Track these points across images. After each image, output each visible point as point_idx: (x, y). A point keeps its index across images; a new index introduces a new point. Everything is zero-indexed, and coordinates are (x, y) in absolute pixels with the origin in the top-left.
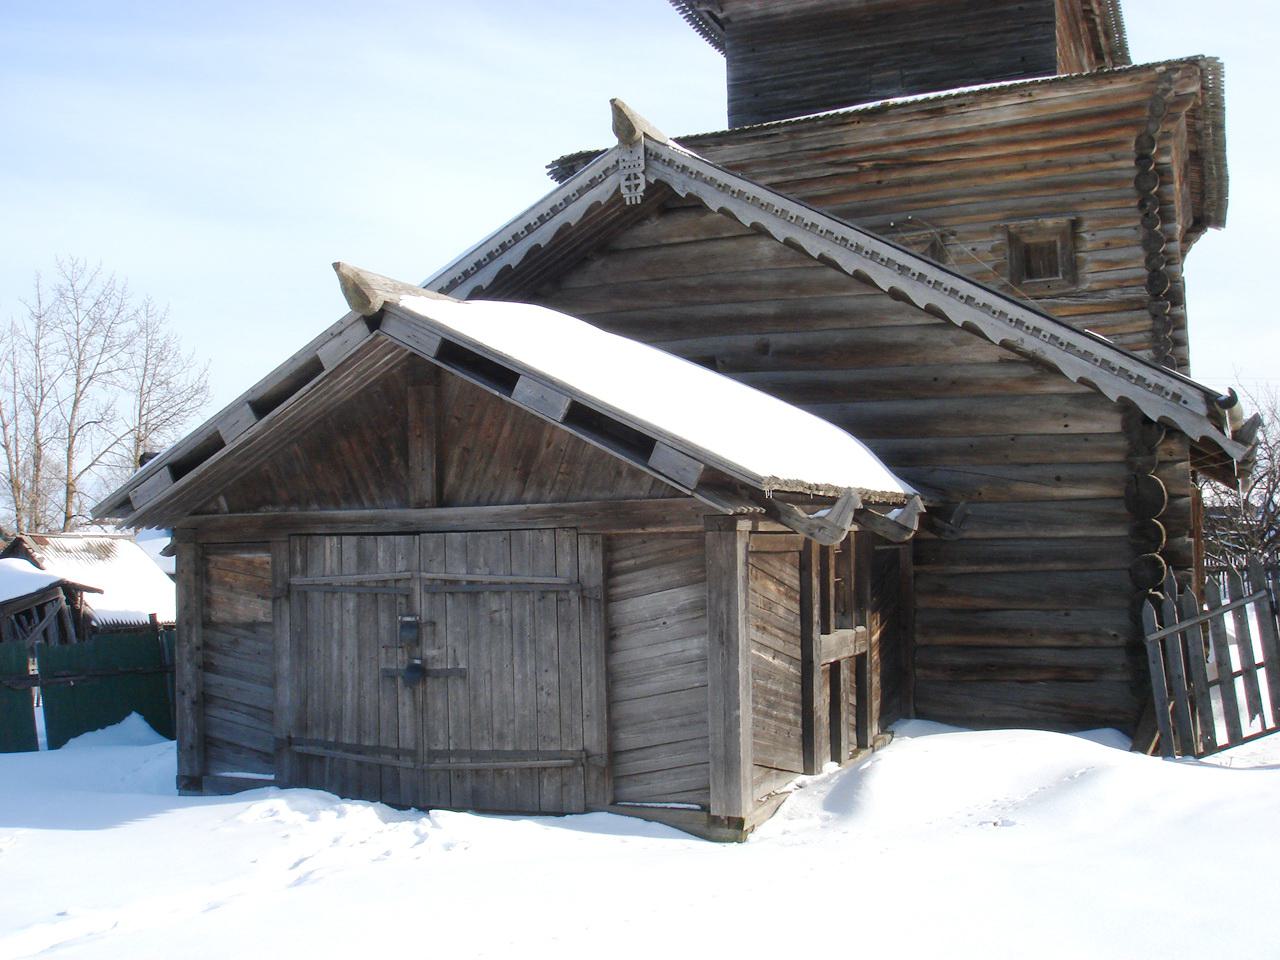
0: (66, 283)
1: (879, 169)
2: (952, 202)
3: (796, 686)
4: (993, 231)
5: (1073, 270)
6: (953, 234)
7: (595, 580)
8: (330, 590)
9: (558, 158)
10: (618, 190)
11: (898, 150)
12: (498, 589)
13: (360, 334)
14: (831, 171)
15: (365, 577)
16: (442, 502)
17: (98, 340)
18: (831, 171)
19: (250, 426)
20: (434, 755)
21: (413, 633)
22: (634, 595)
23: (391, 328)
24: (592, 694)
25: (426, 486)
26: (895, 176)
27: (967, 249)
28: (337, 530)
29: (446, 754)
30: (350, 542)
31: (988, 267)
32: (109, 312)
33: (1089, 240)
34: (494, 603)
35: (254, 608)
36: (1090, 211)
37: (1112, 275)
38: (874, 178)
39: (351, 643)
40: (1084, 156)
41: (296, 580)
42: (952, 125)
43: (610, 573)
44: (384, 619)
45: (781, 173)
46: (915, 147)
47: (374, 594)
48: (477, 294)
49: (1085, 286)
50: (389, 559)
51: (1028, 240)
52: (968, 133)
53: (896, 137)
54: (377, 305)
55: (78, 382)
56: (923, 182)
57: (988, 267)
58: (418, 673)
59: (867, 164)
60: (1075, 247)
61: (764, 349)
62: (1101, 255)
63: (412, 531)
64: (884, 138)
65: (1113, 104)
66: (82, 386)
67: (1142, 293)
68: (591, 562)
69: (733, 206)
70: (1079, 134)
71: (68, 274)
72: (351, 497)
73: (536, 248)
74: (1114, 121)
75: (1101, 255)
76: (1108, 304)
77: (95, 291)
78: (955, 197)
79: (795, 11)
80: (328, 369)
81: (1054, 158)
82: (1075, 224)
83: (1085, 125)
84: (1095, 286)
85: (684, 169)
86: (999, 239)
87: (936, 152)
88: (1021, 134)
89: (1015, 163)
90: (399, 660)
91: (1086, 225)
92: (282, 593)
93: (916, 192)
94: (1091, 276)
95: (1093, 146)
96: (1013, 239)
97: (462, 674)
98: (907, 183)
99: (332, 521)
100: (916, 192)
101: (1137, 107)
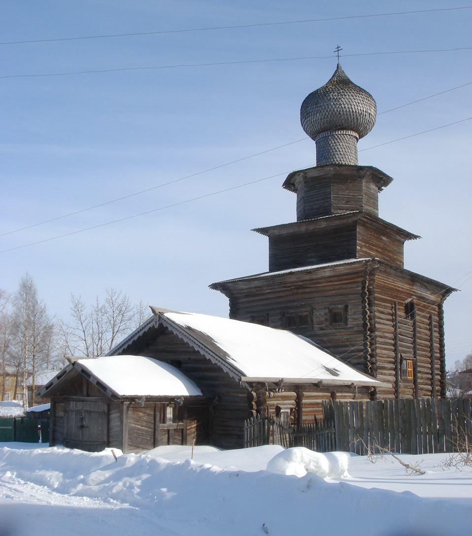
0: (110, 298)
1: (297, 289)
2: (316, 299)
3: (153, 433)
4: (325, 308)
5: (346, 320)
6: (315, 309)
7: (106, 411)
8: (72, 411)
9: (211, 283)
10: (154, 326)
11: (301, 283)
12: (94, 412)
13: (71, 366)
14: (284, 289)
15: (77, 409)
16: (88, 395)
17: (120, 317)
18: (284, 289)
19: (57, 382)
20: (84, 441)
21: (82, 419)
22: (112, 414)
23: (75, 366)
24: (105, 432)
25: (85, 393)
26: (301, 291)
27: (318, 314)
28: (73, 400)
29: (86, 441)
30: (75, 402)
31: (323, 319)
32: (124, 308)
33: (350, 312)
34: (93, 414)
35: (61, 414)
36: (350, 303)
37: (355, 323)
38: (296, 291)
39: (74, 421)
40: (350, 286)
41: (68, 409)
42: (314, 277)
43: (109, 410)
44: (79, 417)
45: (271, 289)
46: (305, 282)
47: (78, 412)
48: (110, 356)
49: (349, 326)
50: (80, 406)
51: (334, 311)
52: (318, 279)
53: (299, 280)
54: (73, 362)
55: (113, 333)
56: (309, 293)
57: (323, 319)
58: (82, 427)
59: (293, 287)
60: (347, 314)
61: (189, 359)
62: (352, 317)
63: (83, 401)
64: (297, 280)
65: (356, 270)
66: (114, 335)
67: (361, 329)
68: (105, 408)
69: (173, 330)
70: (348, 279)
71: (110, 294)
72: (76, 394)
73: (134, 341)
74: (357, 275)
75: (352, 317)
76: (355, 331)
77: (119, 301)
78: (316, 298)
79: (288, 233)
80: (67, 372)
81: (342, 286)
82: (346, 307)
83: (349, 277)
84: (351, 326)
85: (165, 321)
86: (327, 311)
87: (311, 284)
88: (332, 279)
89: (332, 288)
90: (79, 425)
91: (349, 307)
92: (65, 411)
93: (307, 296)
94: (350, 323)
95: (350, 283)
96: (330, 311)
97: (88, 427)
98: (304, 293)
99: (73, 398)
100: (307, 296)
101: (361, 272)
